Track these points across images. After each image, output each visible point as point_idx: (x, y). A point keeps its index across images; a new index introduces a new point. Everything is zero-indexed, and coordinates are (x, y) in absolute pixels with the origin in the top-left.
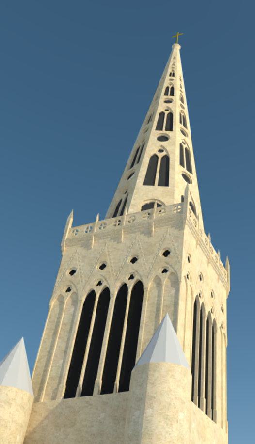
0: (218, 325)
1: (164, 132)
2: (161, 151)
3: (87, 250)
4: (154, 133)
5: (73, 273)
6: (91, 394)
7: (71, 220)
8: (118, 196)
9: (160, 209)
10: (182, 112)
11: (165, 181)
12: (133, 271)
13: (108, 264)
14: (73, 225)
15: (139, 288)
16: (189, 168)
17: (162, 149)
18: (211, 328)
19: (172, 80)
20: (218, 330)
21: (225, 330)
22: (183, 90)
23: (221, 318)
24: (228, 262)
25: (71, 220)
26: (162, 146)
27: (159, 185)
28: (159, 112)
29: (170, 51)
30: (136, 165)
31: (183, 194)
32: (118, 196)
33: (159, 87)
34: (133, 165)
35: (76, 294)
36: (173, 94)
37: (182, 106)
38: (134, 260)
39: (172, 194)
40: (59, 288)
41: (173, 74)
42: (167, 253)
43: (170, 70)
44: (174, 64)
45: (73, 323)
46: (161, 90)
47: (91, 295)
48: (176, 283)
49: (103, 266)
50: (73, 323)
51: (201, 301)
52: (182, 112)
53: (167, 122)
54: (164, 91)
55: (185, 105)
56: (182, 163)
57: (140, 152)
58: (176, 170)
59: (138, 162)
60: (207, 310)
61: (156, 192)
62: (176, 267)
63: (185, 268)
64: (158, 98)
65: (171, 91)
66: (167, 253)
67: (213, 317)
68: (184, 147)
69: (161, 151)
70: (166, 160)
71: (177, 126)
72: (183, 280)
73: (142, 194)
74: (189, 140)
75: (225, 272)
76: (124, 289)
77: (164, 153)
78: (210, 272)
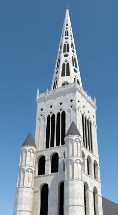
0: (92, 122)
1: (66, 53)
2: (66, 61)
3: (45, 103)
4: (63, 54)
5: (42, 110)
6: (58, 171)
7: (38, 91)
8: (54, 81)
9: (68, 85)
10: (72, 42)
11: (68, 74)
12: (61, 108)
13: (53, 106)
14: (40, 93)
15: (64, 113)
16: (76, 67)
17: (66, 60)
18: (90, 123)
19: (67, 28)
20: (92, 124)
21: (95, 124)
22: (72, 32)
23: (93, 120)
24: (95, 99)
25: (38, 91)
26: (66, 59)
27: (67, 76)
28: (65, 31)
29: (65, 12)
30: (58, 68)
31: (75, 77)
32: (54, 81)
33: (63, 32)
34: (57, 68)
35: (44, 117)
36: (68, 35)
37: (71, 39)
38: (61, 104)
39: (71, 79)
40: (38, 116)
41: (67, 25)
42: (71, 101)
43: (66, 23)
44: (67, 20)
45: (44, 126)
46: (63, 33)
47: (49, 116)
48: (75, 111)
49: (51, 107)
50: (44, 126)
51: (85, 115)
52: (72, 42)
53: (66, 48)
54: (66, 25)
55: (73, 38)
56: (73, 65)
57: (59, 61)
58: (72, 68)
59: (56, 85)
60: (87, 118)
61: (66, 79)
62: (75, 105)
63: (78, 105)
64: (64, 28)
65: (67, 34)
66: (71, 101)
67: (90, 120)
68: (74, 57)
69: (66, 61)
70: (68, 64)
71: (70, 49)
72: (77, 110)
73: (62, 80)
74: (75, 54)
75: (94, 104)
76: (59, 114)
77: (67, 62)
78: (87, 104)
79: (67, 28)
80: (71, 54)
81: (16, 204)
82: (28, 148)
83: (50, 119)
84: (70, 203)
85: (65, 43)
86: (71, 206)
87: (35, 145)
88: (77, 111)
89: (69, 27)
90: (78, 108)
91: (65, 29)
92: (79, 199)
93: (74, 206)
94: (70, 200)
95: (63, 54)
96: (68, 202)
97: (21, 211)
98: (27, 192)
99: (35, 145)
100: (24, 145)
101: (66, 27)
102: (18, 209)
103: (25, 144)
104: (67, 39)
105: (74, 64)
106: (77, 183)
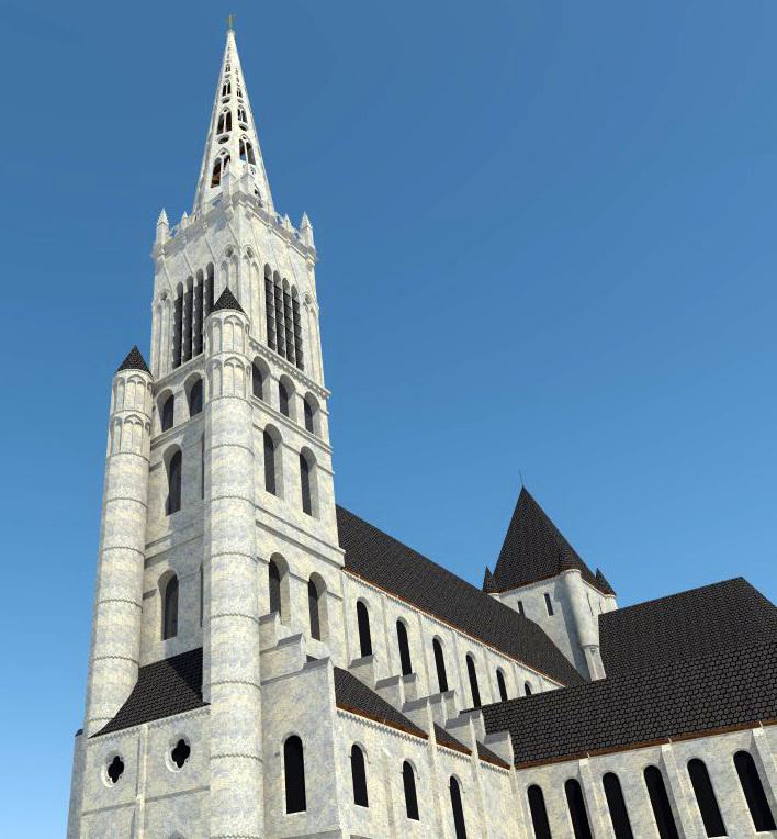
68: (245, 142)
70: (229, 115)
79: (227, 76)
80: (236, 134)
81: (88, 703)
82: (127, 374)
83: (174, 634)
84: (214, 678)
85: (219, 156)
86: (214, 684)
87: (146, 369)
88: (243, 263)
89: (232, 72)
90: (245, 257)
91: (224, 79)
92: (240, 737)
93: (222, 554)
94: (213, 669)
95: (216, 137)
96: (209, 678)
97: (116, 499)
98: (117, 670)
99: (146, 369)
100: (122, 368)
101: (224, 74)
102: (97, 655)
103: (126, 365)
104: (226, 101)
105: (242, 115)
106: (232, 692)
